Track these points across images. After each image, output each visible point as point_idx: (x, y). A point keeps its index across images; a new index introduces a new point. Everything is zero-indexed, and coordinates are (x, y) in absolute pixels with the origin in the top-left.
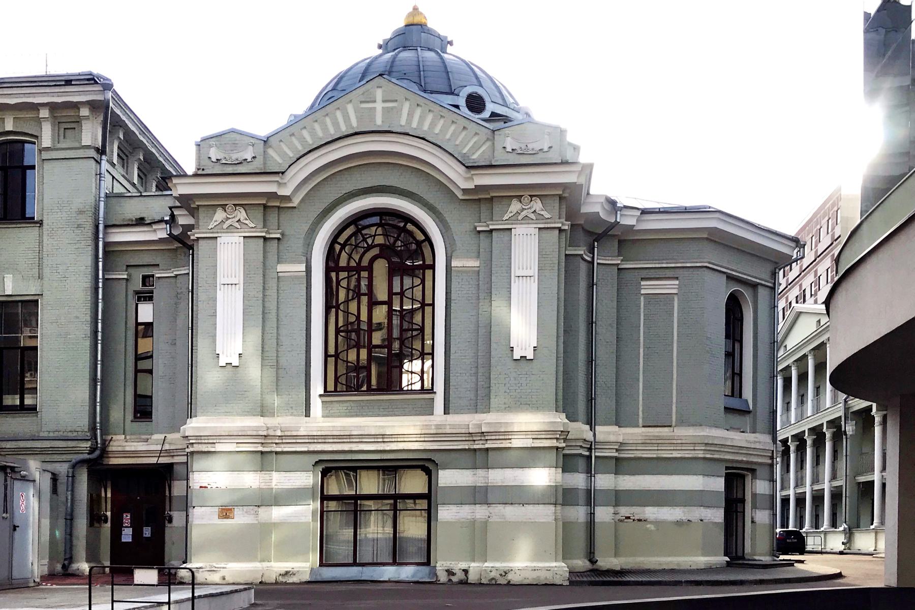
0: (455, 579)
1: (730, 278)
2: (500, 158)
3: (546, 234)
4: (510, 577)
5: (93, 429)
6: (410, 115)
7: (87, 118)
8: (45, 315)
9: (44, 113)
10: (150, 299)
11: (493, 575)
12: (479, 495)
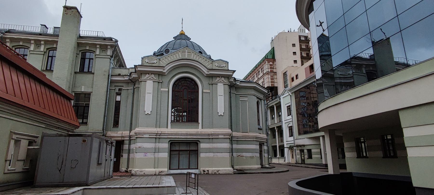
0: (205, 173)
1: (257, 98)
2: (214, 68)
3: (225, 85)
4: (219, 172)
5: (103, 130)
6: (194, 56)
7: (109, 48)
8: (92, 98)
9: (98, 46)
10: (120, 95)
11: (215, 171)
12: (209, 150)
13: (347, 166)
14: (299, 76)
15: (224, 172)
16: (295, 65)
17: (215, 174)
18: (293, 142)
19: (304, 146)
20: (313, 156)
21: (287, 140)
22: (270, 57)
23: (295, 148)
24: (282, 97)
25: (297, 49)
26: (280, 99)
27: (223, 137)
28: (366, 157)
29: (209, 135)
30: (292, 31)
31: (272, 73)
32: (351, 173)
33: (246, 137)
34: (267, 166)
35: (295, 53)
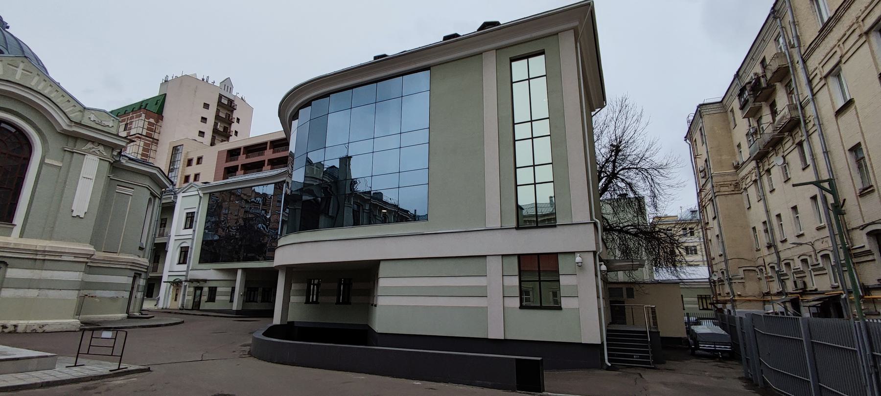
0: (6, 330)
2: (85, 121)
11: (35, 327)
13: (824, 320)
14: (204, 160)
15: (58, 328)
16: (200, 139)
17: (34, 332)
18: (184, 273)
19: (205, 281)
20: (217, 298)
21: (171, 267)
22: (155, 109)
23: (185, 284)
24: (180, 196)
25: (211, 114)
26: (176, 197)
27: (72, 259)
28: (316, 302)
29: (36, 252)
30: (210, 82)
31: (151, 139)
32: (293, 322)
33: (110, 261)
34: (137, 314)
35: (204, 120)
